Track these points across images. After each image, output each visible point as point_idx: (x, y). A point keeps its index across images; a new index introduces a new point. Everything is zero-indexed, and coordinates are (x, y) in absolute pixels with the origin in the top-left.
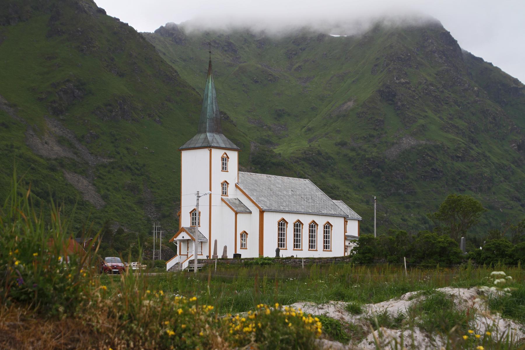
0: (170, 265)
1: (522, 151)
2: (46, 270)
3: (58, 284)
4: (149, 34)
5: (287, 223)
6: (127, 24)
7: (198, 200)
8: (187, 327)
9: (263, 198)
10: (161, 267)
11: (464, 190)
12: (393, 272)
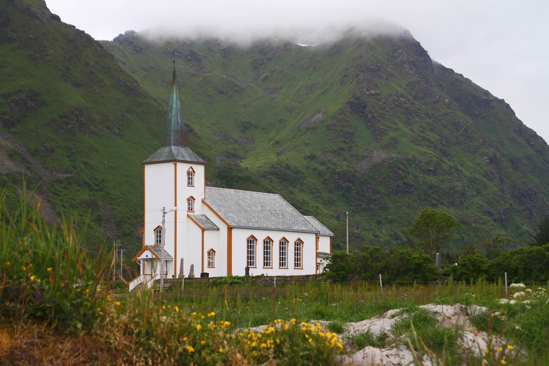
0: (132, 286)
1: (493, 165)
2: (63, 285)
3: (75, 300)
4: (107, 42)
5: (257, 240)
6: (84, 32)
7: (164, 216)
8: (206, 343)
9: (231, 214)
10: (122, 288)
11: (437, 205)
12: (369, 290)
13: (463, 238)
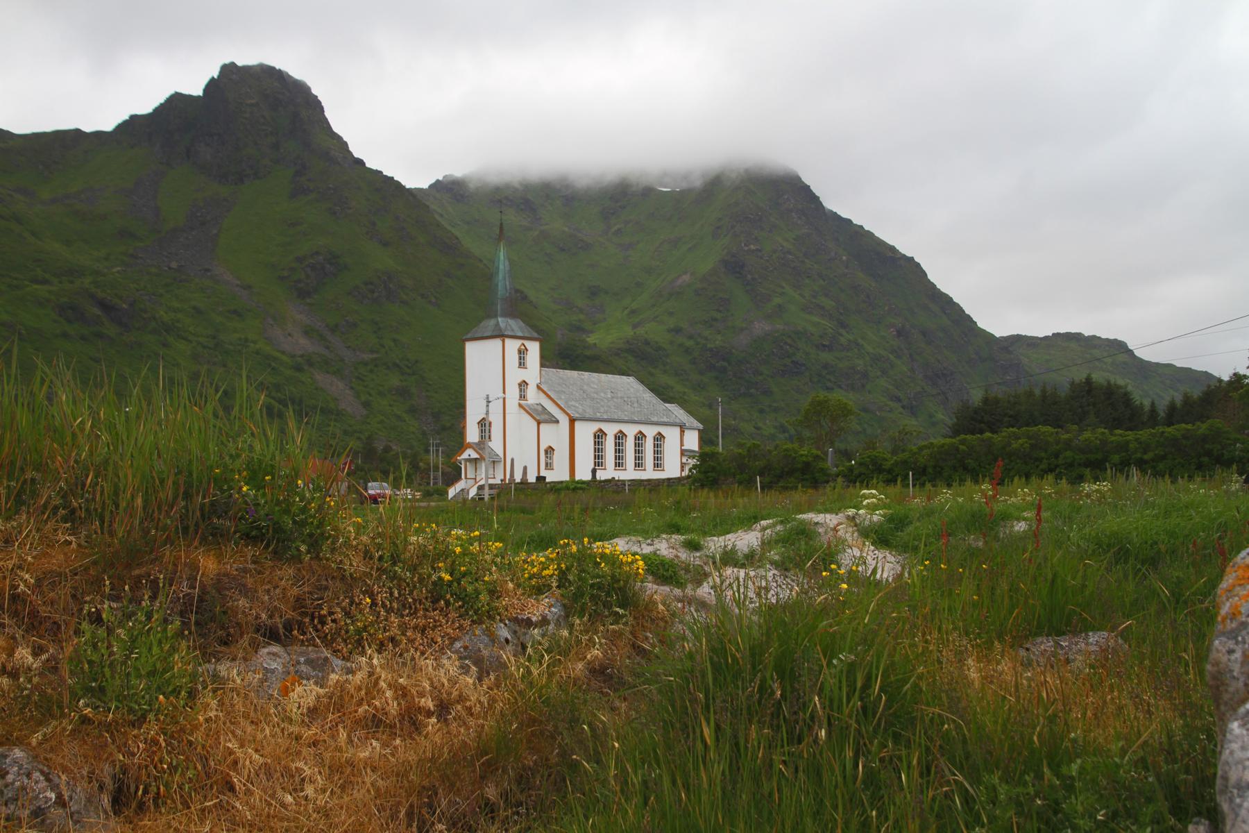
0: (452, 492)
12: (743, 496)
13: (864, 430)
